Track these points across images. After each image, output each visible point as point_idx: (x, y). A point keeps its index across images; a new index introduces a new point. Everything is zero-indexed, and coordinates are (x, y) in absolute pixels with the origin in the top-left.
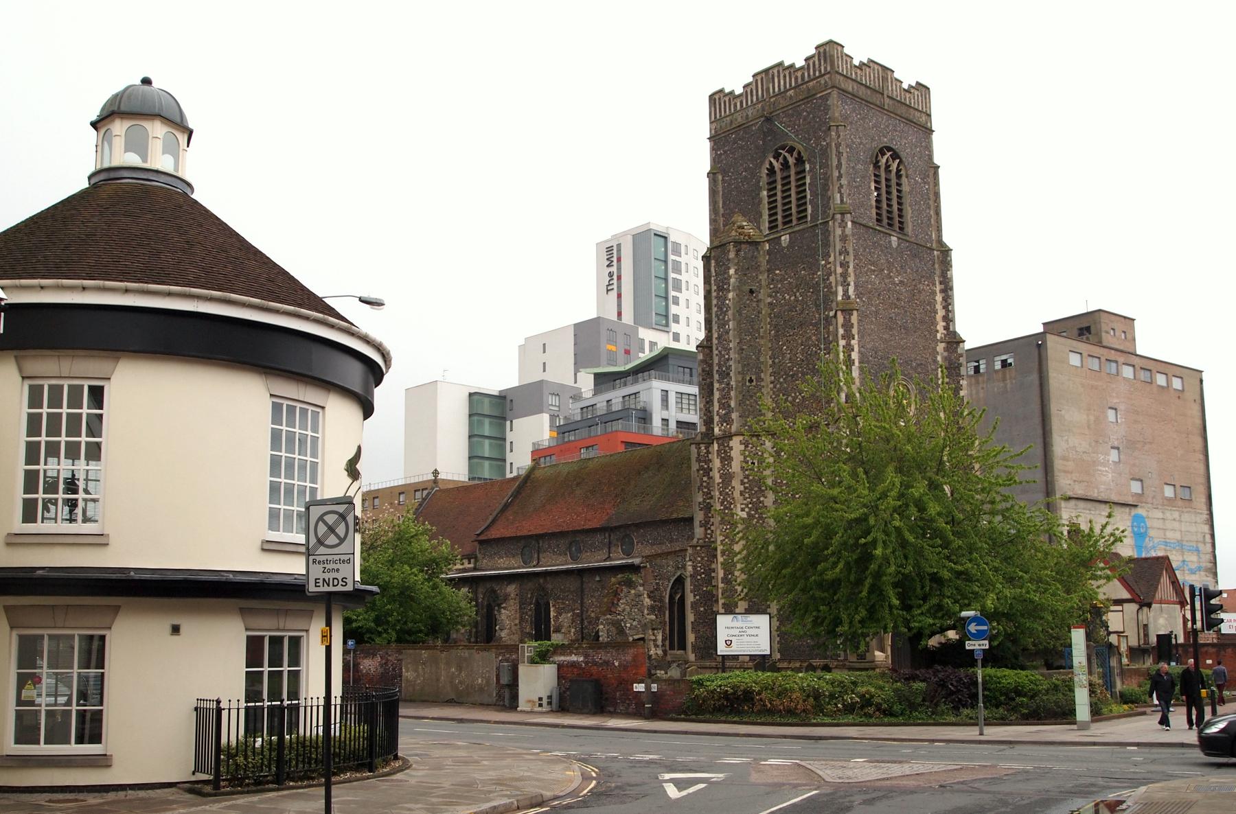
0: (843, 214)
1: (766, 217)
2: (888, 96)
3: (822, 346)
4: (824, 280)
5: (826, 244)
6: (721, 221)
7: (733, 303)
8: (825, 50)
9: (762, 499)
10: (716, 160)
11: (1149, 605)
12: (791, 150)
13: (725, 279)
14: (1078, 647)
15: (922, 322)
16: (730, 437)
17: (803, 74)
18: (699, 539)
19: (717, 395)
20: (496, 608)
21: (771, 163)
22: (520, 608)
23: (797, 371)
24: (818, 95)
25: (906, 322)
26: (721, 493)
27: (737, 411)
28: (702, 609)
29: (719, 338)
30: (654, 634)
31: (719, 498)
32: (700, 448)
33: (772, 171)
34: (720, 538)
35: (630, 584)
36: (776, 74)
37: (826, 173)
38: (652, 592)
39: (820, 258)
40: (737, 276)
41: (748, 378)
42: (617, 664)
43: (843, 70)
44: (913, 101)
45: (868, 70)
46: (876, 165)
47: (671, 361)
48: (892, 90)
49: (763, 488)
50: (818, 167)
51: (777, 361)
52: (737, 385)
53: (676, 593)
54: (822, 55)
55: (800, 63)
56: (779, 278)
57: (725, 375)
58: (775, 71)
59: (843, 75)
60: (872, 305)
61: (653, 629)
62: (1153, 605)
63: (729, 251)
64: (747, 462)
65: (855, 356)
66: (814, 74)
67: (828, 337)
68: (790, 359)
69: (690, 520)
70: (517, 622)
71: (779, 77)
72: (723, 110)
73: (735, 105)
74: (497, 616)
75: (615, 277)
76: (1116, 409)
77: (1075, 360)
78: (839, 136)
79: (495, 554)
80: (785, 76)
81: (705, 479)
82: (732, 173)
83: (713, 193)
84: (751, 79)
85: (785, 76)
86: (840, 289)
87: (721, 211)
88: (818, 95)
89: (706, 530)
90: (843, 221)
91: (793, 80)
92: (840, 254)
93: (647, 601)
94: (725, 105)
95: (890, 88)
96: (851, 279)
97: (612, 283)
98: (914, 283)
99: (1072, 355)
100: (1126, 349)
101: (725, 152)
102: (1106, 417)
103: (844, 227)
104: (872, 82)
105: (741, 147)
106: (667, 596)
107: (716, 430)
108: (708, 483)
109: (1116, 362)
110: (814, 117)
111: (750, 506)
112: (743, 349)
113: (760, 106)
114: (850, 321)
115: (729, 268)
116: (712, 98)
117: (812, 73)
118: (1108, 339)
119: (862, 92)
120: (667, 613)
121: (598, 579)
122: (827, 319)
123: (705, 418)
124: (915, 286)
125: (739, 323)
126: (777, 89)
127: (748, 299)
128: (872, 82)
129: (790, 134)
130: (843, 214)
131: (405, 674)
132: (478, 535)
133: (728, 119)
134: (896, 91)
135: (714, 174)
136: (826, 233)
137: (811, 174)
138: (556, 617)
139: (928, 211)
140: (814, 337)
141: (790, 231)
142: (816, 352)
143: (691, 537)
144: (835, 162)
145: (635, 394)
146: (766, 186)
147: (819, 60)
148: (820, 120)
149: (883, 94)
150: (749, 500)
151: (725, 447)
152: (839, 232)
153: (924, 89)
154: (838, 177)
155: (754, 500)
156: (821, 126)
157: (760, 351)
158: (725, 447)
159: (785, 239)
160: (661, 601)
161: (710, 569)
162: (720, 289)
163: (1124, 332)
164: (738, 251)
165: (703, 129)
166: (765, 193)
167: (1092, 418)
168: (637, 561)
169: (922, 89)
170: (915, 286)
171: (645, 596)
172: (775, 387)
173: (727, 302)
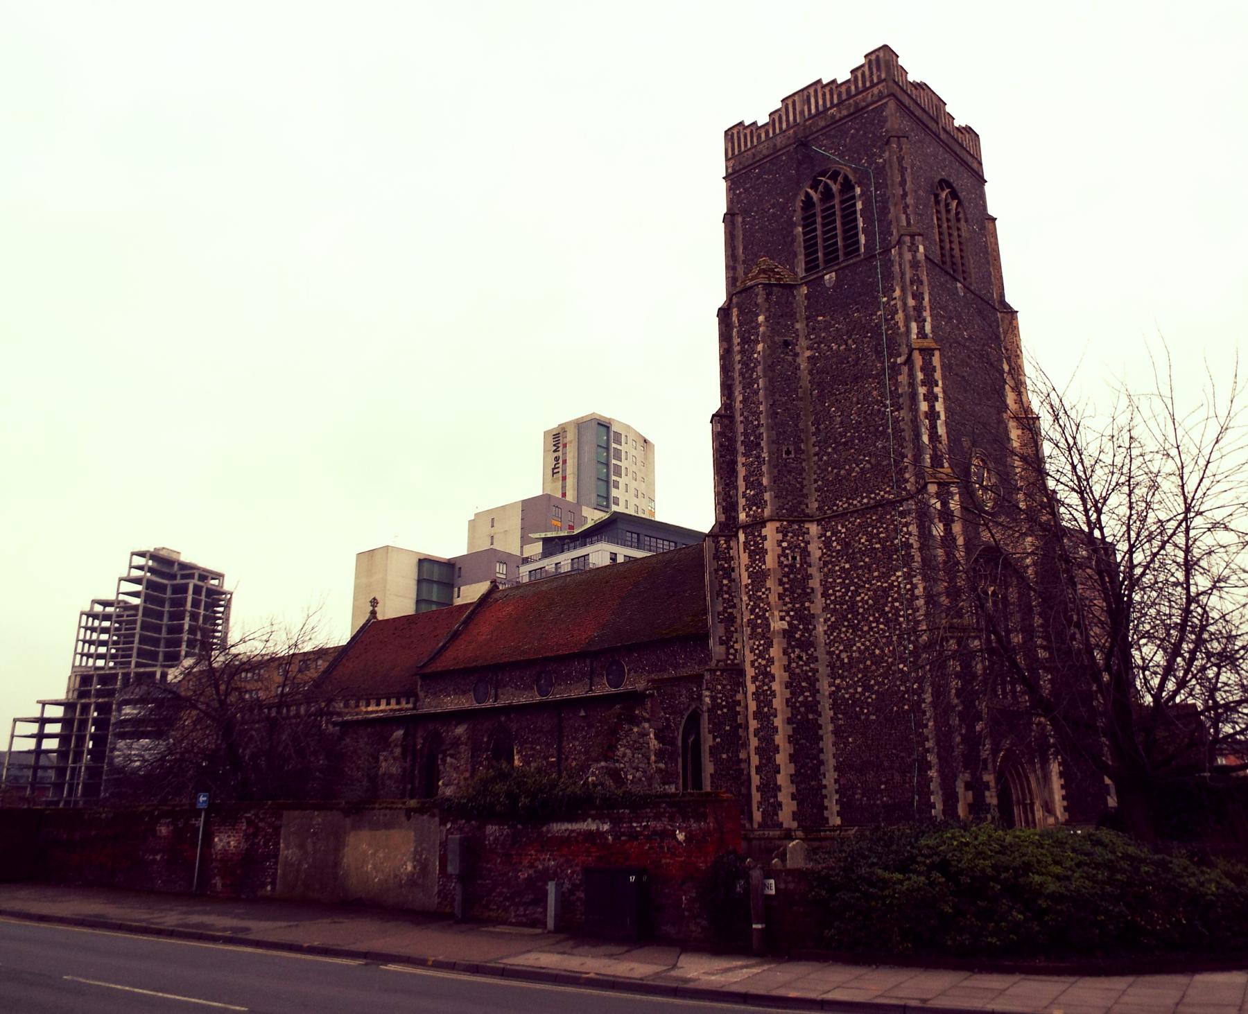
0: (912, 236)
3: (888, 402)
4: (886, 320)
5: (888, 276)
6: (741, 270)
7: (764, 357)
8: (878, 56)
9: (807, 604)
10: (731, 202)
12: (834, 176)
13: (753, 328)
16: (763, 524)
18: (718, 661)
19: (742, 472)
21: (807, 194)
22: (473, 757)
23: (853, 438)
24: (871, 108)
26: (750, 598)
27: (771, 490)
28: (724, 756)
29: (744, 401)
31: (748, 605)
32: (718, 542)
33: (808, 203)
34: (749, 657)
35: (636, 721)
37: (885, 195)
39: (881, 295)
41: (785, 449)
42: (681, 837)
47: (620, 525)
49: (809, 590)
50: (873, 189)
52: (769, 456)
54: (874, 63)
57: (752, 446)
58: (812, 91)
63: (757, 295)
64: (786, 556)
65: (939, 406)
68: (842, 422)
73: (759, 137)
74: (441, 768)
75: (560, 461)
79: (441, 691)
80: (824, 95)
81: (725, 582)
82: (756, 212)
84: (779, 105)
85: (824, 95)
86: (914, 326)
88: (871, 108)
89: (728, 649)
90: (913, 244)
91: (835, 97)
92: (912, 283)
93: (654, 743)
97: (556, 469)
101: (746, 190)
105: (768, 182)
106: (680, 738)
107: (742, 516)
108: (729, 588)
110: (865, 133)
111: (792, 613)
112: (777, 413)
113: (791, 131)
115: (758, 315)
116: (729, 134)
120: (680, 760)
121: (582, 713)
123: (724, 504)
127: (782, 352)
129: (832, 157)
130: (912, 236)
133: (749, 153)
136: (888, 264)
137: (864, 198)
140: (875, 392)
141: (836, 268)
142: (879, 410)
143: (709, 657)
145: (584, 556)
146: (802, 223)
150: (790, 605)
151: (755, 536)
152: (908, 256)
154: (902, 196)
155: (797, 606)
157: (798, 415)
158: (755, 536)
160: (672, 742)
161: (734, 701)
162: (745, 340)
164: (769, 295)
165: (718, 167)
166: (800, 229)
171: (652, 735)
173: (756, 356)
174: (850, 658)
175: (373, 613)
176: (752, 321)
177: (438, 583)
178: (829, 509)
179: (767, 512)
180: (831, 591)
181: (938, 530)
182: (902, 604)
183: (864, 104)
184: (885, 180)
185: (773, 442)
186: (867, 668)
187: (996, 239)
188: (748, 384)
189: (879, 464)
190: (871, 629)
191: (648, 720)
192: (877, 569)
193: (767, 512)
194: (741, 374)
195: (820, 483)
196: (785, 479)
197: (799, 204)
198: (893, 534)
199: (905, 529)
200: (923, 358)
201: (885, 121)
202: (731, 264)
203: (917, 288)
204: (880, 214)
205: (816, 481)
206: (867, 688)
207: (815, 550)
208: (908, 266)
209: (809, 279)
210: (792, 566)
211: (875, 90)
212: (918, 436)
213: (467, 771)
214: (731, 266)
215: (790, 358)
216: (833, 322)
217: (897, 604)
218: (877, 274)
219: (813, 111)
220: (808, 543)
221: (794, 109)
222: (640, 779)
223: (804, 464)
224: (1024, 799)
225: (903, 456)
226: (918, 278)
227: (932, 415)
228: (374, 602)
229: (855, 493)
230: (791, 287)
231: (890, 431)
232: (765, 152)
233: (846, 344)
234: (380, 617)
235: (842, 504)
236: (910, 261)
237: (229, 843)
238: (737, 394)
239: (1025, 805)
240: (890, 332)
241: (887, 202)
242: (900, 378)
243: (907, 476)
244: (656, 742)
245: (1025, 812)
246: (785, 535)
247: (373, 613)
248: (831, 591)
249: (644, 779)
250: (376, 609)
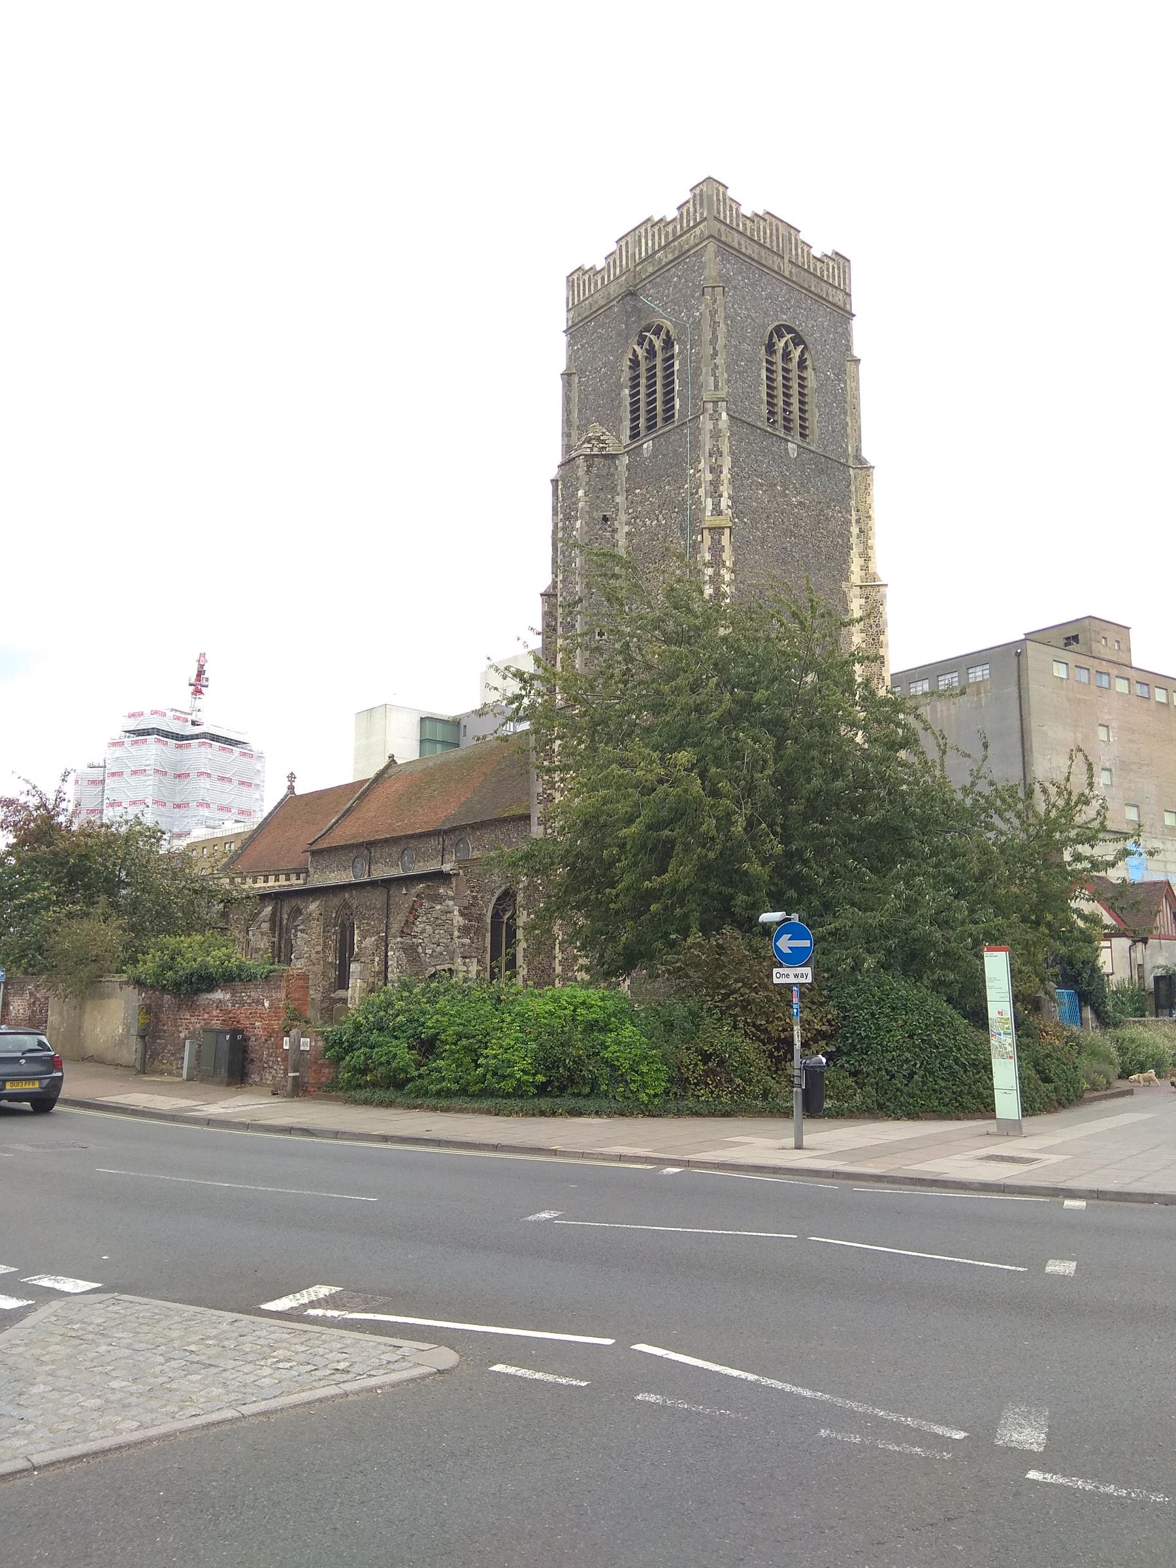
0: (715, 403)
1: (627, 424)
2: (790, 262)
4: (692, 494)
5: (696, 445)
7: (581, 535)
8: (702, 190)
10: (572, 357)
11: (1145, 941)
12: (657, 333)
14: (996, 984)
15: (828, 558)
20: (293, 931)
25: (807, 556)
30: (464, 964)
33: (635, 363)
35: (438, 899)
36: (643, 234)
37: (699, 353)
38: (466, 908)
40: (587, 499)
43: (725, 217)
44: (825, 273)
45: (762, 222)
46: (770, 348)
48: (797, 255)
50: (689, 347)
53: (504, 911)
55: (672, 214)
58: (643, 231)
59: (725, 224)
60: (757, 529)
61: (464, 957)
62: (1150, 941)
69: (527, 818)
70: (319, 948)
71: (646, 237)
72: (581, 292)
76: (1107, 727)
77: (1060, 671)
78: (715, 301)
79: (327, 866)
80: (653, 236)
83: (567, 399)
85: (653, 236)
91: (663, 237)
93: (458, 920)
94: (584, 290)
95: (794, 252)
98: (819, 507)
99: (1127, 808)
100: (1120, 661)
101: (583, 346)
102: (1096, 735)
104: (768, 240)
106: (489, 914)
109: (1109, 674)
110: (686, 282)
114: (719, 541)
116: (570, 282)
117: (685, 225)
118: (1099, 648)
119: (750, 250)
120: (488, 935)
124: (821, 510)
128: (768, 240)
130: (715, 403)
131: (50, 1019)
132: (311, 844)
134: (803, 257)
135: (569, 375)
138: (360, 942)
139: (842, 416)
144: (708, 336)
146: (629, 384)
147: (694, 205)
149: (783, 258)
153: (841, 261)
159: (647, 446)
160: (480, 918)
163: (1118, 642)
165: (559, 319)
166: (627, 391)
167: (1079, 735)
168: (446, 868)
169: (841, 261)
170: (821, 510)
171: (456, 913)
173: (574, 533)
175: (291, 788)
177: (442, 742)
183: (687, 247)
187: (858, 383)
191: (452, 899)
196: (596, 661)
200: (712, 538)
201: (704, 268)
203: (716, 459)
209: (631, 448)
211: (697, 231)
213: (319, 945)
215: (608, 534)
216: (648, 495)
219: (643, 254)
221: (627, 252)
222: (441, 954)
226: (718, 449)
228: (292, 777)
230: (614, 457)
232: (602, 302)
233: (657, 519)
234: (298, 792)
236: (711, 431)
237: (19, 1010)
240: (694, 507)
241: (700, 362)
244: (461, 919)
247: (291, 788)
249: (445, 953)
250: (293, 784)
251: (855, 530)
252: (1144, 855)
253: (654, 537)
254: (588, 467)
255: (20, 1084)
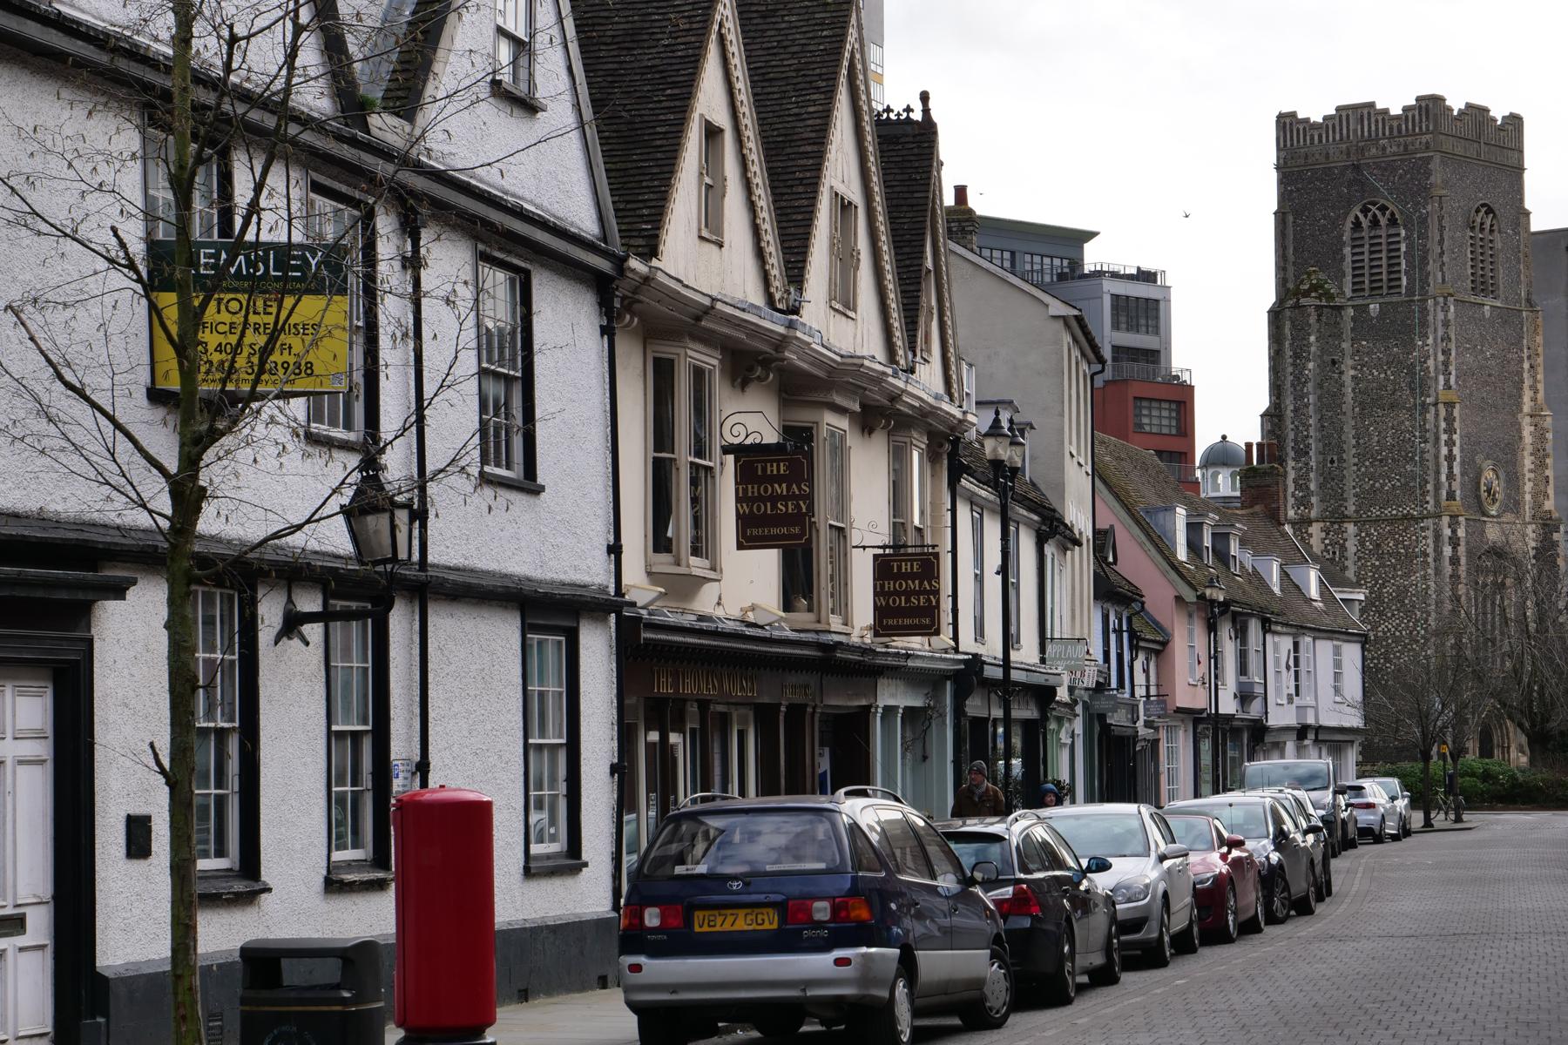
4: (1420, 362)
5: (1424, 324)
8: (1427, 105)
10: (1283, 197)
12: (1383, 209)
16: (1310, 522)
17: (1400, 125)
21: (1357, 217)
24: (1418, 155)
27: (1317, 495)
29: (1296, 410)
33: (1357, 225)
36: (1366, 116)
41: (1329, 459)
50: (1415, 236)
51: (1361, 441)
52: (1317, 466)
54: (1424, 110)
55: (1396, 110)
56: (1366, 350)
58: (1365, 112)
63: (1309, 315)
64: (1328, 552)
65: (1456, 451)
66: (1414, 130)
67: (1424, 424)
68: (1378, 442)
71: (1369, 119)
80: (1377, 121)
84: (1333, 112)
86: (1441, 378)
87: (1291, 258)
88: (1418, 155)
92: (1442, 340)
96: (1452, 368)
101: (1298, 190)
103: (1445, 310)
107: (1291, 513)
110: (1412, 178)
112: (1324, 427)
113: (1344, 146)
115: (1309, 335)
122: (1423, 404)
125: (1320, 398)
126: (1366, 134)
129: (1381, 189)
136: (1424, 311)
147: (1420, 115)
148: (1420, 183)
152: (1441, 316)
156: (1416, 187)
159: (1374, 308)
172: (1359, 470)
174: (1375, 636)
176: (1304, 339)
178: (1365, 513)
179: (1313, 514)
180: (1363, 582)
181: (1447, 551)
182: (1418, 599)
184: (1426, 231)
185: (1320, 453)
186: (1388, 645)
188: (1299, 397)
189: (1407, 484)
190: (1393, 615)
192: (1401, 569)
193: (1313, 514)
194: (1292, 385)
195: (1358, 490)
196: (1329, 486)
197: (1349, 225)
198: (1415, 544)
199: (1424, 541)
202: (1282, 264)
204: (1419, 260)
205: (1354, 488)
206: (1387, 660)
207: (1352, 547)
208: (1440, 324)
210: (1332, 560)
212: (1438, 473)
214: (1281, 268)
217: (1414, 599)
218: (1414, 318)
220: (1346, 540)
223: (1345, 472)
224: (1503, 743)
225: (1427, 482)
227: (1450, 458)
229: (1387, 504)
230: (1340, 308)
231: (1417, 458)
235: (1375, 512)
238: (1288, 402)
239: (1503, 747)
242: (1428, 416)
243: (1428, 498)
245: (1503, 753)
246: (1328, 534)
248: (1363, 582)
251: (1526, 365)
252: (282, 460)
253: (1382, 387)
254: (1319, 316)
255: (719, 920)
